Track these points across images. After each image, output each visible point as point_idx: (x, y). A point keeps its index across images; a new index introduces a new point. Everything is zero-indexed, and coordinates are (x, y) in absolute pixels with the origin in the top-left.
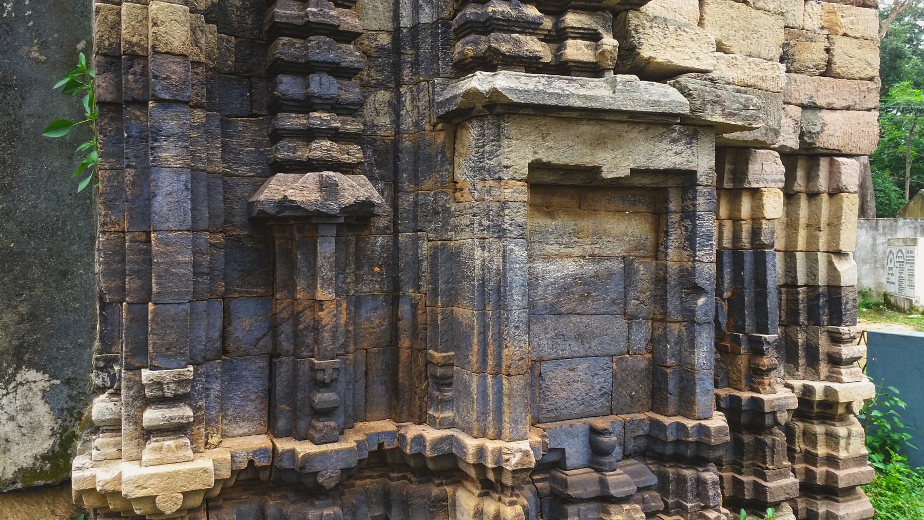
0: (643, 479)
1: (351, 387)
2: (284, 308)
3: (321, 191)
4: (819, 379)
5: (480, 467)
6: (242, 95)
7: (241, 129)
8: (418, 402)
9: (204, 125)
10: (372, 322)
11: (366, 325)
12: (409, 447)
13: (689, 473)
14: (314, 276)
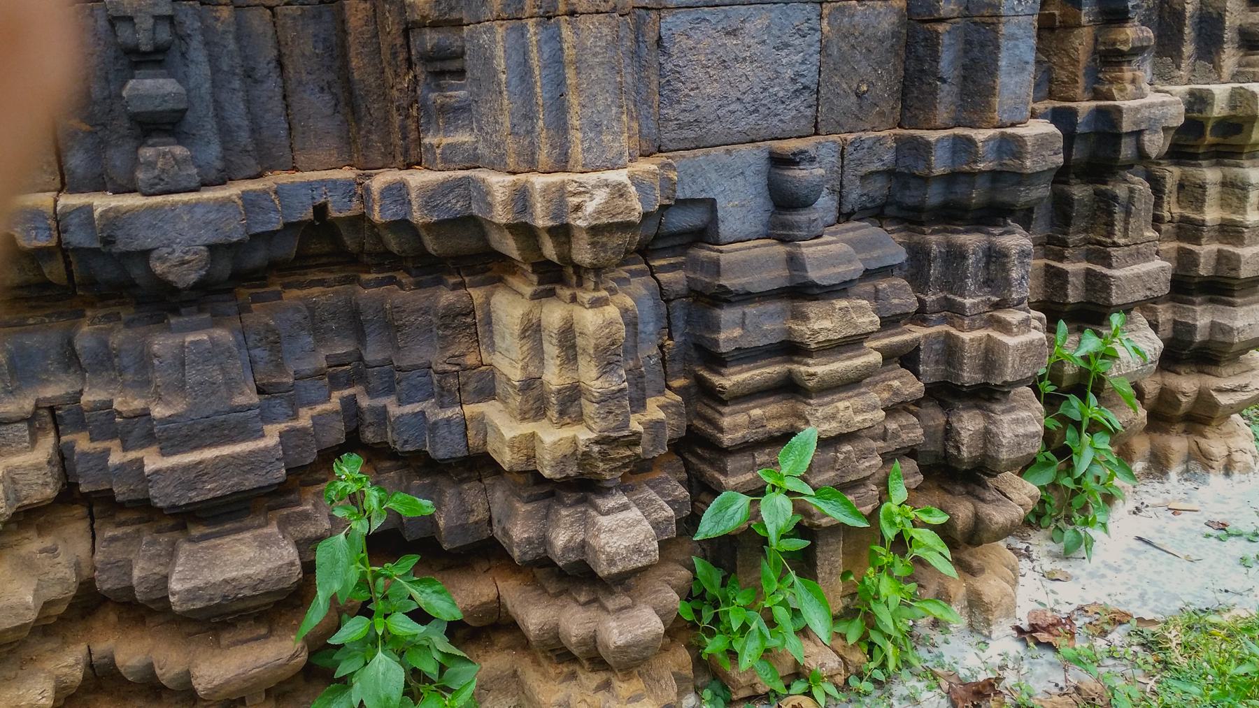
0: (875, 254)
4: (1219, 80)
5: (524, 231)
8: (397, 119)
12: (377, 208)
13: (972, 241)
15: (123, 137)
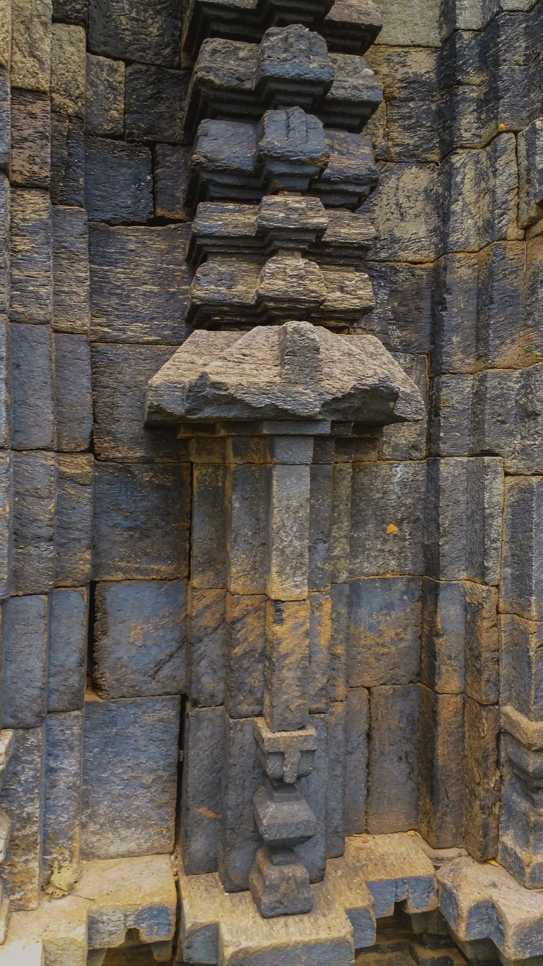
1: (339, 771)
2: (207, 607)
3: (282, 364)
6: (137, 180)
7: (132, 246)
9: (44, 226)
10: (381, 634)
11: (370, 639)
12: (463, 926)
14: (266, 545)
15: (245, 839)
